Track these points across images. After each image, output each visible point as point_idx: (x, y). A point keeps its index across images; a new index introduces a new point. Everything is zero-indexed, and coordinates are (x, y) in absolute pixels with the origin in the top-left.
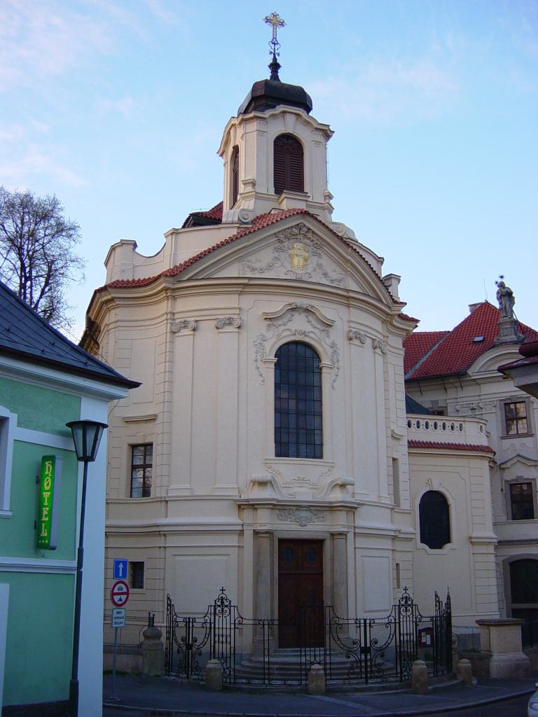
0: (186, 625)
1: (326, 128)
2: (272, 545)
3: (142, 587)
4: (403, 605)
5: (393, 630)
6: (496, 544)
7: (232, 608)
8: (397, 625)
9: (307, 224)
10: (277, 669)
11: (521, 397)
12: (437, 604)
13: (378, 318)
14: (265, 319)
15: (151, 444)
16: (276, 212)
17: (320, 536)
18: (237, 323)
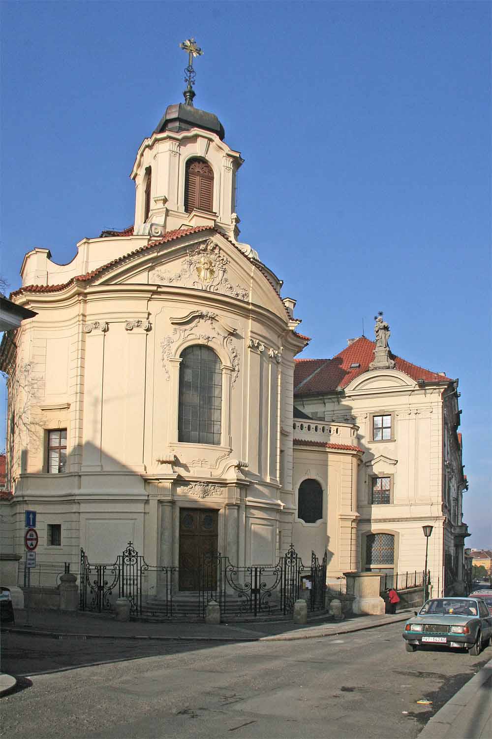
0: (98, 572)
2: (173, 513)
3: (60, 545)
4: (289, 558)
5: (279, 576)
7: (139, 558)
8: (283, 573)
10: (178, 606)
12: (314, 560)
13: (275, 332)
14: (172, 323)
15: (65, 429)
16: (186, 228)
17: (216, 507)
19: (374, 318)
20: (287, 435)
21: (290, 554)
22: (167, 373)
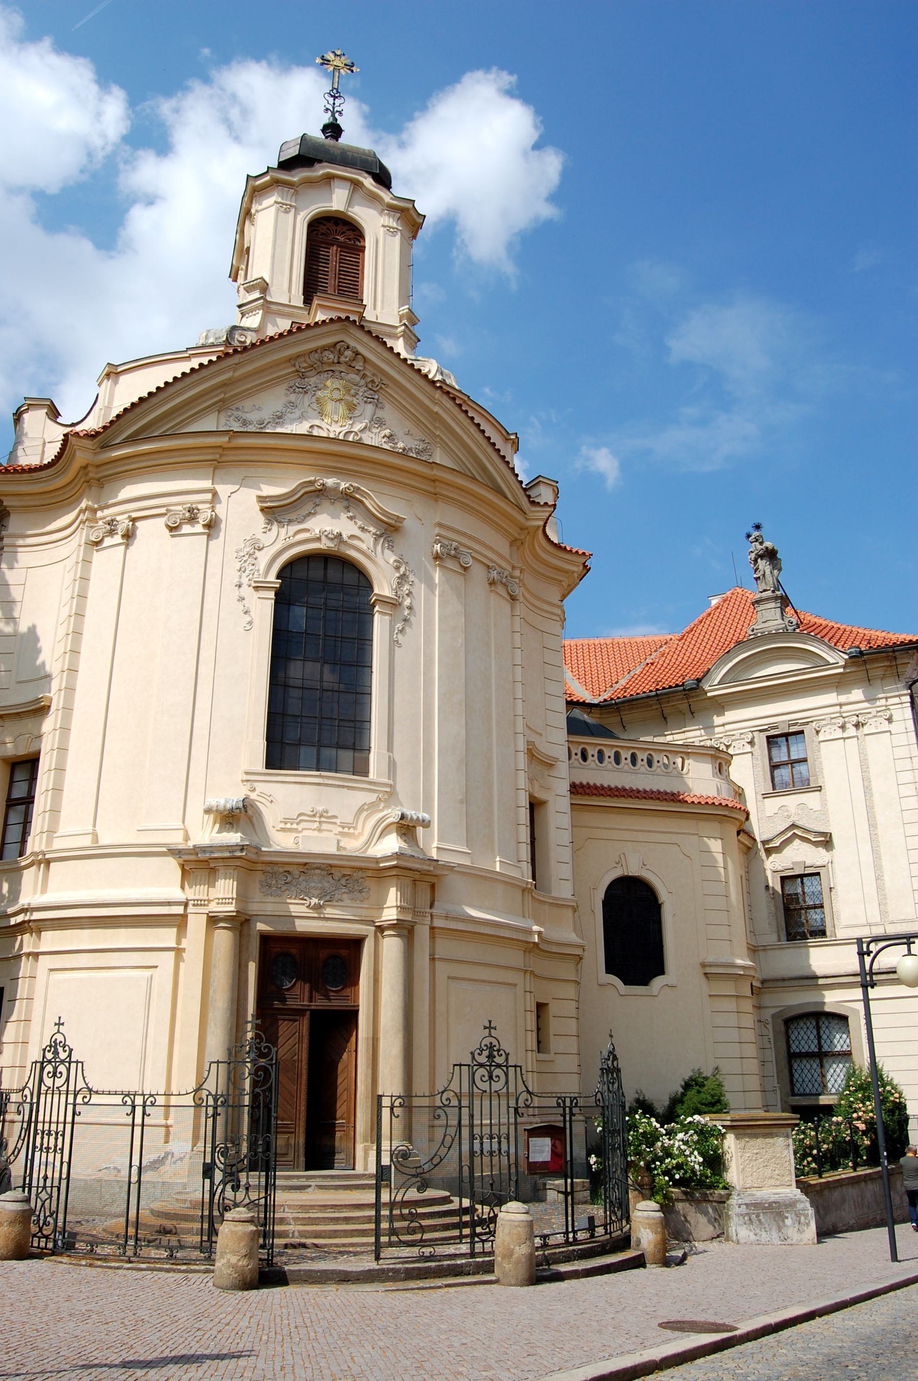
1: (410, 206)
4: (481, 1065)
6: (756, 984)
9: (352, 344)
11: (795, 724)
18: (205, 516)
19: (744, 535)
20: (552, 765)
21: (486, 1053)
22: (246, 613)
